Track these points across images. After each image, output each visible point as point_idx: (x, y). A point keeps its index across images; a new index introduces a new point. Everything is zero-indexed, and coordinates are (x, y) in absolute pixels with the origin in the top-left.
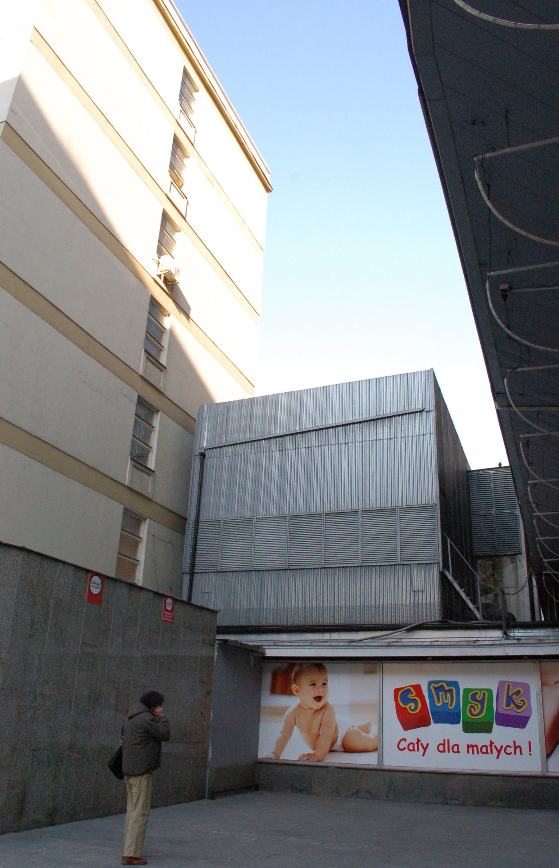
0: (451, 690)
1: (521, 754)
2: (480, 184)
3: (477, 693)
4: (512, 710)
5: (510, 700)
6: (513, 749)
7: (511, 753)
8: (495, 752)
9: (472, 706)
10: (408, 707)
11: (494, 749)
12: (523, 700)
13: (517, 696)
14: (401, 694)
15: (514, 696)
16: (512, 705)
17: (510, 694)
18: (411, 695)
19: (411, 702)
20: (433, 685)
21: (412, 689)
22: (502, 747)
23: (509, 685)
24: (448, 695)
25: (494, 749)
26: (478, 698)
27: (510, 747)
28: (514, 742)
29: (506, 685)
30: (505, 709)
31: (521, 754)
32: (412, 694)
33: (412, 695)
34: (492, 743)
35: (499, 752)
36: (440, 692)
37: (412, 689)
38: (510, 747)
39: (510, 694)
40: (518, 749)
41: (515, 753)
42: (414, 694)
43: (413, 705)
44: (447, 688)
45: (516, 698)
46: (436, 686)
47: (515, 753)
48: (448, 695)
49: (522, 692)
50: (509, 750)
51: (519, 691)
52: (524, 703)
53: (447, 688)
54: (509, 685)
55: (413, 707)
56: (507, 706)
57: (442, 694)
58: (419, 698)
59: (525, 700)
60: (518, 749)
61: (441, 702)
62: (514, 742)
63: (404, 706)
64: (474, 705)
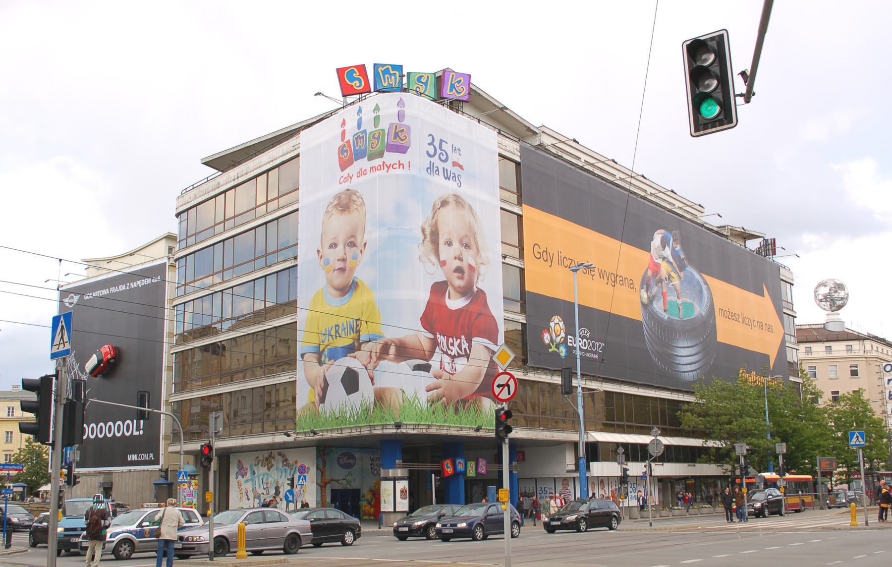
1: (403, 168)
2: (169, 368)
3: (423, 76)
4: (398, 142)
5: (396, 135)
6: (397, 166)
7: (396, 168)
8: (386, 168)
9: (373, 143)
10: (353, 84)
11: (385, 166)
12: (462, 88)
13: (459, 84)
14: (347, 74)
15: (457, 84)
16: (454, 91)
17: (453, 83)
19: (355, 80)
21: (355, 69)
22: (390, 164)
23: (396, 126)
24: (393, 77)
25: (385, 166)
26: (422, 81)
27: (396, 164)
28: (399, 161)
29: (395, 126)
30: (392, 141)
31: (403, 168)
32: (356, 73)
33: (356, 75)
34: (384, 162)
35: (388, 168)
36: (386, 74)
38: (396, 164)
39: (453, 83)
40: (401, 166)
41: (399, 168)
42: (358, 74)
43: (357, 83)
45: (458, 86)
46: (383, 70)
47: (399, 168)
48: (393, 77)
50: (395, 166)
51: (461, 80)
52: (406, 138)
53: (392, 72)
54: (396, 126)
55: (358, 85)
56: (394, 139)
57: (388, 77)
58: (363, 78)
59: (464, 87)
60: (401, 166)
61: (387, 83)
62: (399, 161)
63: (350, 84)
64: (419, 86)
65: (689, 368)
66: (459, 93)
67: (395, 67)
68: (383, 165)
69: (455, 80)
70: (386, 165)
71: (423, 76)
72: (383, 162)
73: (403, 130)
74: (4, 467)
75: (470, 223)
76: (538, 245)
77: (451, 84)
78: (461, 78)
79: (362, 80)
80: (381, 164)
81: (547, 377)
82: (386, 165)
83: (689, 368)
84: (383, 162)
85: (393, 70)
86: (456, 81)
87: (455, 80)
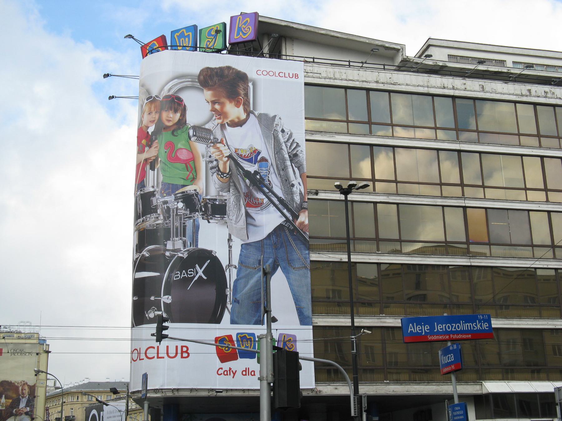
0: (189, 36)
9: (208, 41)
12: (249, 28)
13: (245, 25)
16: (241, 34)
18: (249, 21)
20: (177, 34)
21: (226, 338)
23: (285, 336)
24: (187, 39)
37: (226, 338)
44: (186, 34)
45: (244, 27)
46: (178, 34)
48: (187, 39)
49: (249, 21)
53: (186, 34)
54: (285, 336)
65: (458, 413)
66: (244, 34)
67: (188, 29)
68: (230, 371)
69: (242, 21)
70: (232, 371)
71: (213, 29)
72: (230, 368)
73: (290, 340)
74: (432, 328)
75: (145, 126)
76: (281, 72)
77: (239, 27)
78: (248, 19)
79: (152, 99)
80: (228, 369)
81: (397, 320)
82: (232, 371)
83: (458, 413)
84: (230, 368)
85: (187, 33)
86: (242, 23)
87: (242, 21)
